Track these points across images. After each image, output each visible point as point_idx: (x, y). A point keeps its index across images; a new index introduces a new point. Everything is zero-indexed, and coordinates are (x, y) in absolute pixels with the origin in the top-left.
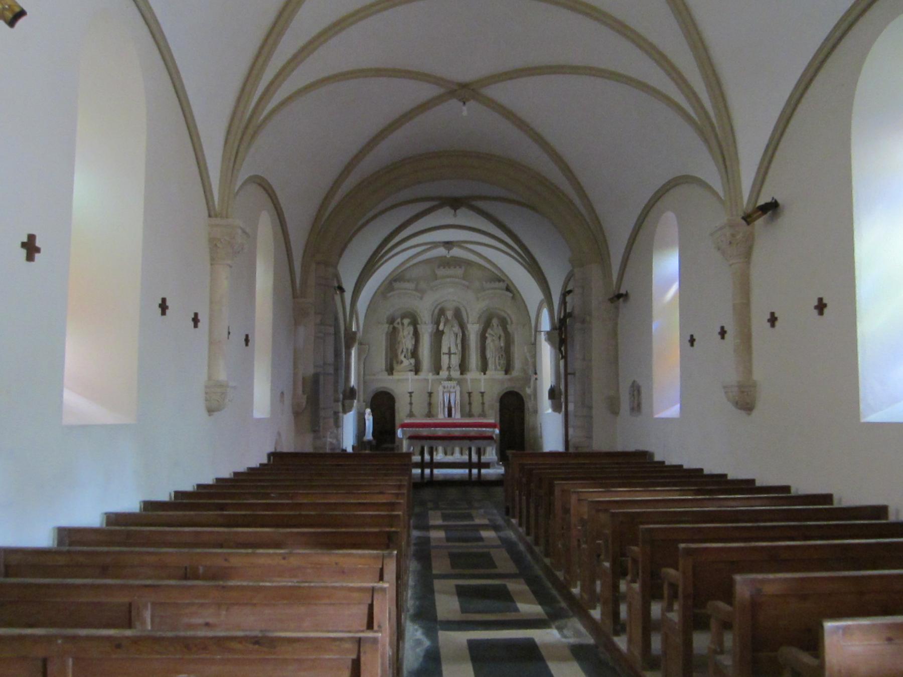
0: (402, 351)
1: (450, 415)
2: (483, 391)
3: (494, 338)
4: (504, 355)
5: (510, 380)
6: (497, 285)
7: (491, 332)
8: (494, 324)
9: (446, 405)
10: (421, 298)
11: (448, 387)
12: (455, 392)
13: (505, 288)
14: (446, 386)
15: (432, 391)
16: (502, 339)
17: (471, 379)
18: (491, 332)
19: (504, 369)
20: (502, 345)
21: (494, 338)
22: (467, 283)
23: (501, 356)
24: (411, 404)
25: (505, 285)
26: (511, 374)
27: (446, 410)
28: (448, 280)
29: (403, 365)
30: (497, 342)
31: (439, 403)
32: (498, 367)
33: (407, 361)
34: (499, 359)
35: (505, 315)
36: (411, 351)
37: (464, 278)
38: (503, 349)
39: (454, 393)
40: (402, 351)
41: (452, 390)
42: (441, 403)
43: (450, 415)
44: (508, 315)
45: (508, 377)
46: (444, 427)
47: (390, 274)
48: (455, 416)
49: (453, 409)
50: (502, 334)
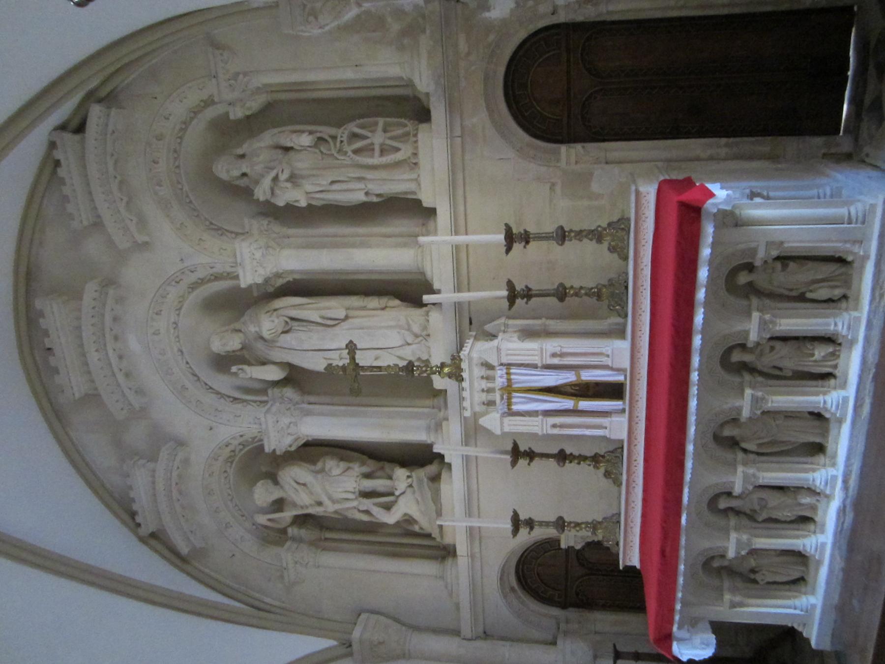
0: (367, 512)
1: (614, 391)
2: (500, 237)
3: (283, 177)
4: (353, 127)
5: (453, 107)
6: (69, 170)
7: (267, 182)
8: (236, 173)
9: (568, 403)
10: (181, 443)
11: (489, 391)
12: (509, 365)
13: (77, 137)
14: (484, 397)
15: (509, 447)
16: (240, 151)
17: (458, 289)
18: (267, 182)
19: (410, 126)
20: (305, 140)
21: (283, 177)
22: (90, 290)
23: (359, 144)
24: (562, 236)
25: (68, 136)
26: (427, 95)
27: (585, 404)
28: (94, 357)
29: (414, 512)
30: (303, 163)
31: (556, 431)
32: (399, 156)
33: (402, 501)
34: (368, 150)
35: (199, 126)
36: (368, 476)
37: (77, 295)
38: (326, 131)
39: (513, 370)
40: (367, 512)
41: (500, 381)
42: (554, 426)
43: (614, 391)
44: (195, 112)
45: (438, 113)
46: (681, 465)
47: (397, 193)
48: (619, 370)
49: (587, 376)
50: (268, 138)
